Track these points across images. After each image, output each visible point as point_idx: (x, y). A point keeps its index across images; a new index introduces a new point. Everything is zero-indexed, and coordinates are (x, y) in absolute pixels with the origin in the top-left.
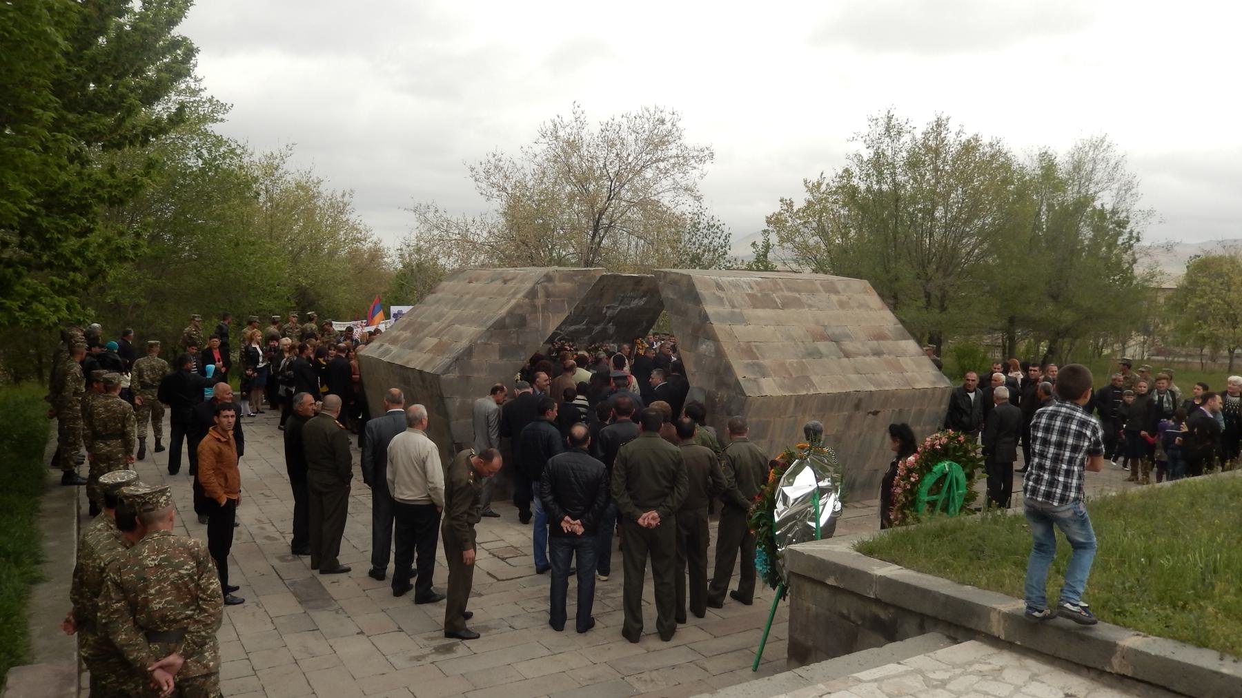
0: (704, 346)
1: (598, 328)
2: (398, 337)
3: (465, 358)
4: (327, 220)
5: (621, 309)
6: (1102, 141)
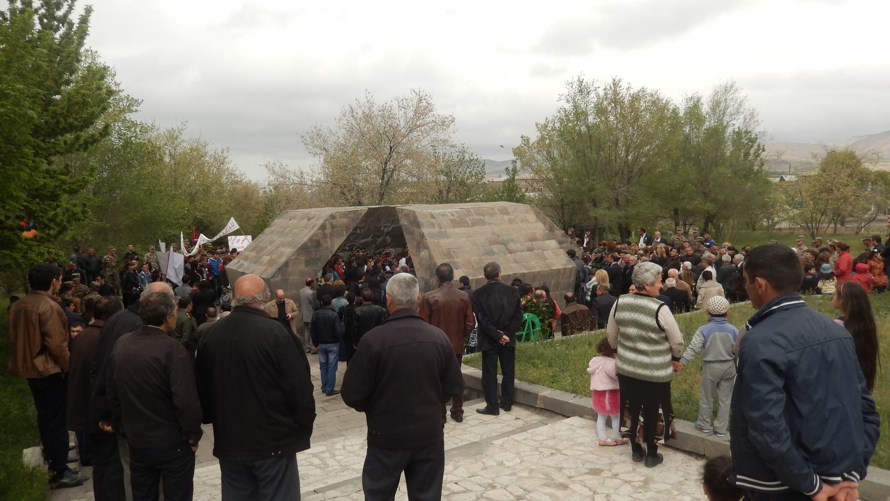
0: (423, 253)
1: (380, 240)
6: (732, 87)
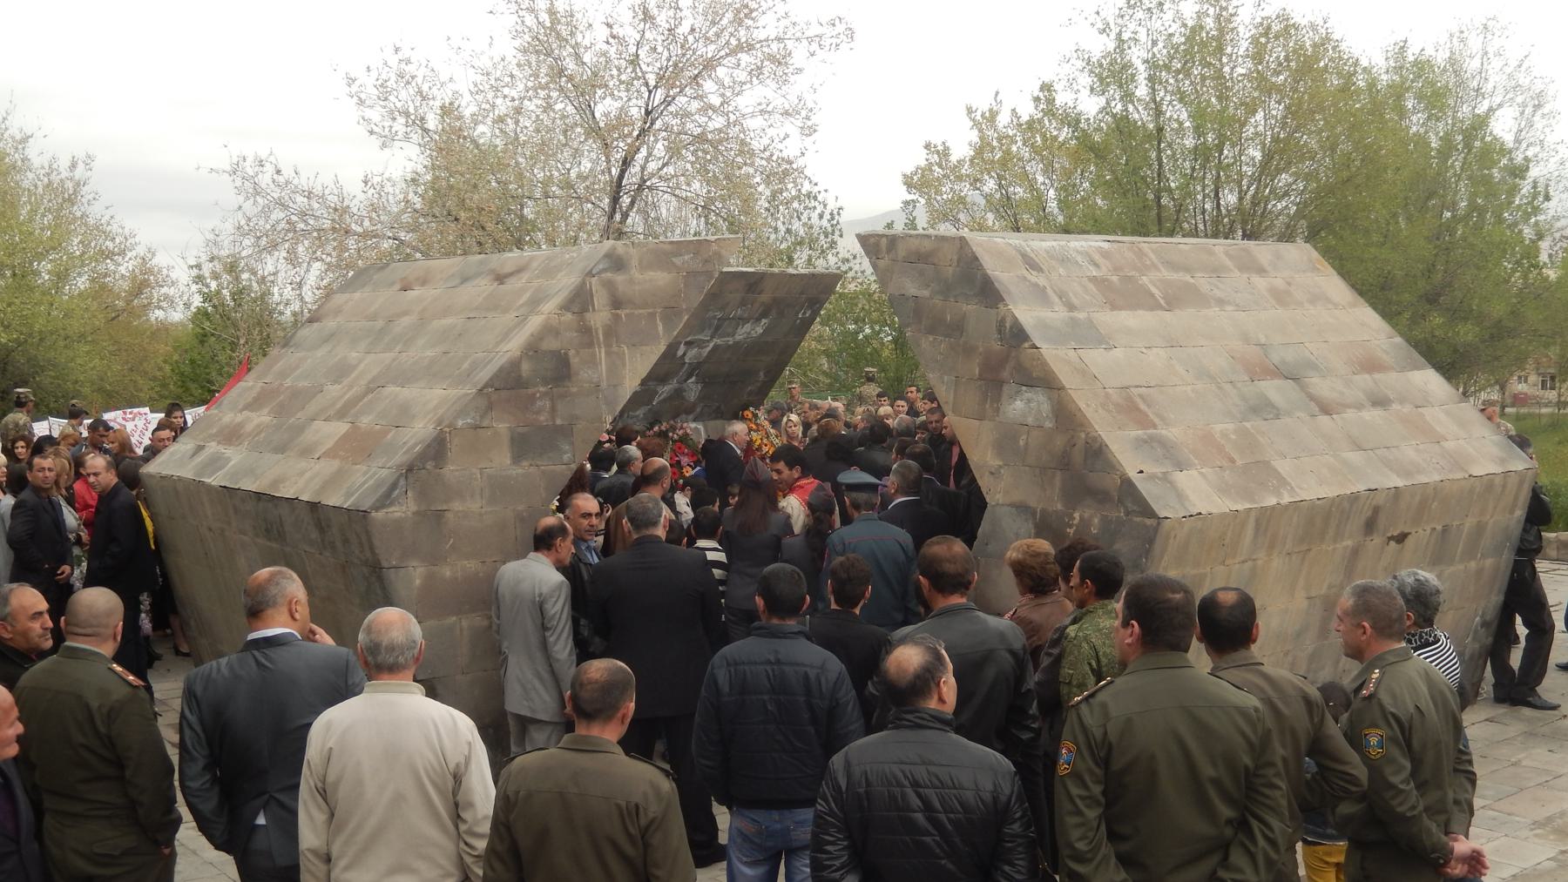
0: (1019, 404)
1: (665, 390)
2: (241, 425)
3: (429, 465)
4: (44, 216)
5: (716, 347)
